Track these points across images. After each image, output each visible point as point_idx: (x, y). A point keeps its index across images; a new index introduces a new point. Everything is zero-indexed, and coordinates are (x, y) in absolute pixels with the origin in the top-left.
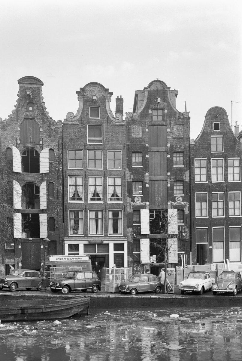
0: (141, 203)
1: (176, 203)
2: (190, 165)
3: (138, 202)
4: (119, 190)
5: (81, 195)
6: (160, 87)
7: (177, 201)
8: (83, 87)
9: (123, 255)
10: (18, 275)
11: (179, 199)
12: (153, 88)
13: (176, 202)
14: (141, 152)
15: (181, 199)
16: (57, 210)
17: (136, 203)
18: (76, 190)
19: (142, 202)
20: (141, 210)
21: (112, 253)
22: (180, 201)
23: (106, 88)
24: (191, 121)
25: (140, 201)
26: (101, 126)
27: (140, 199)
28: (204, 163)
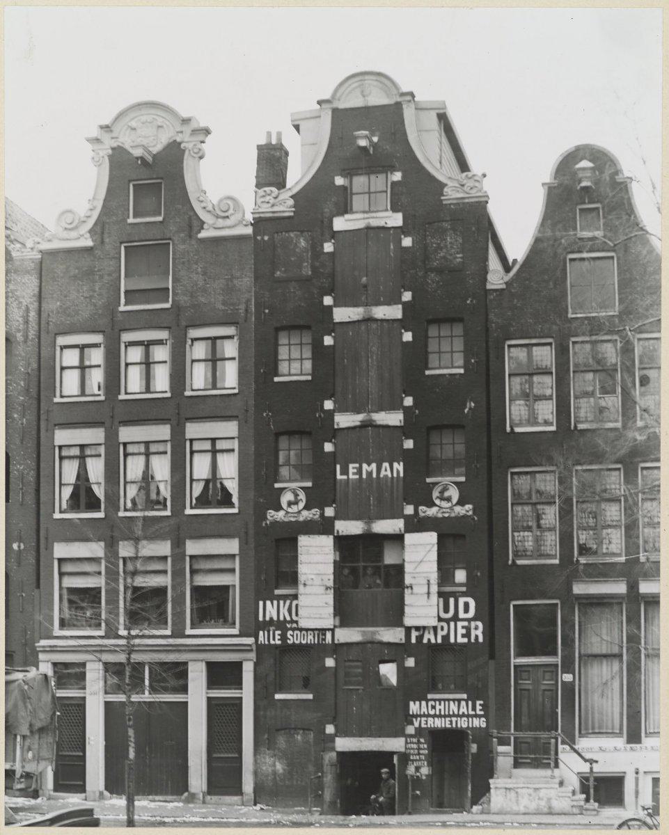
0: (305, 514)
1: (435, 509)
2: (486, 374)
3: (294, 509)
4: (229, 468)
5: (99, 492)
6: (377, 98)
7: (437, 502)
8: (107, 122)
9: (237, 704)
10: (643, 407)
11: (446, 494)
12: (353, 101)
13: (435, 505)
14: (308, 327)
15: (454, 493)
16: (19, 547)
17: (287, 513)
18: (82, 475)
19: (307, 507)
20: (299, 538)
21: (197, 695)
22: (449, 499)
23: (185, 115)
24: (494, 210)
25: (301, 505)
26: (169, 244)
27: (302, 496)
28: (545, 355)
